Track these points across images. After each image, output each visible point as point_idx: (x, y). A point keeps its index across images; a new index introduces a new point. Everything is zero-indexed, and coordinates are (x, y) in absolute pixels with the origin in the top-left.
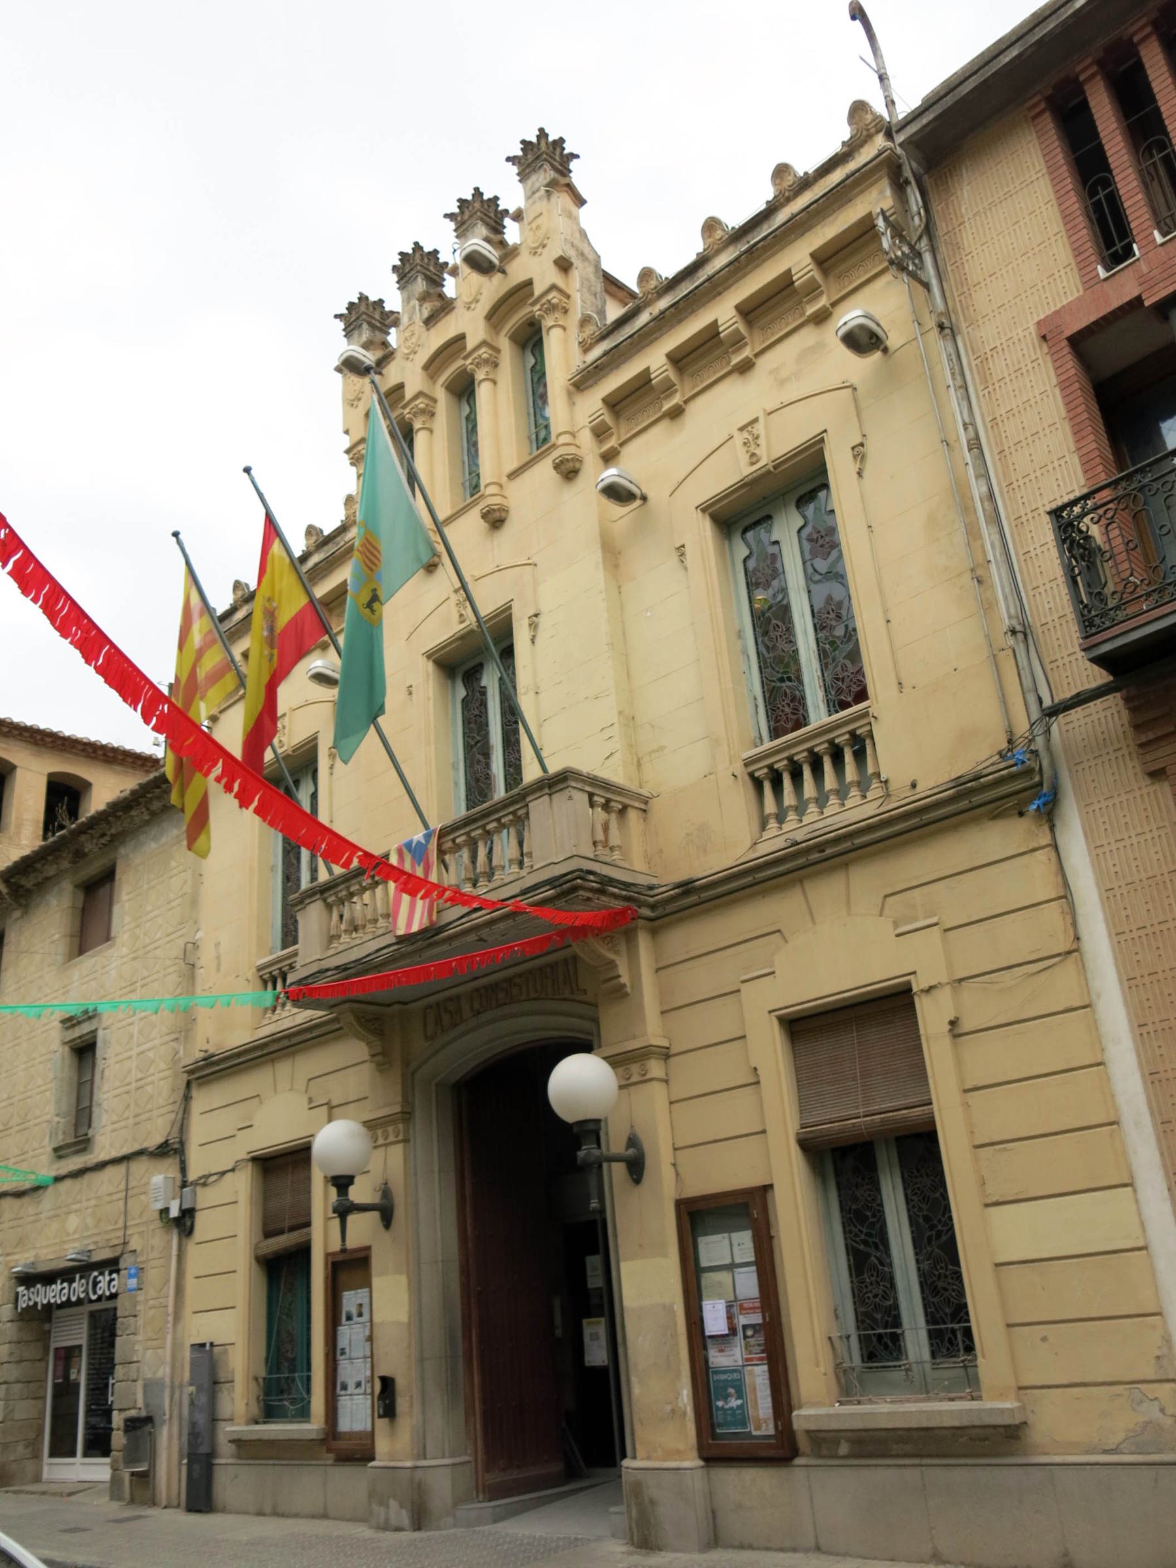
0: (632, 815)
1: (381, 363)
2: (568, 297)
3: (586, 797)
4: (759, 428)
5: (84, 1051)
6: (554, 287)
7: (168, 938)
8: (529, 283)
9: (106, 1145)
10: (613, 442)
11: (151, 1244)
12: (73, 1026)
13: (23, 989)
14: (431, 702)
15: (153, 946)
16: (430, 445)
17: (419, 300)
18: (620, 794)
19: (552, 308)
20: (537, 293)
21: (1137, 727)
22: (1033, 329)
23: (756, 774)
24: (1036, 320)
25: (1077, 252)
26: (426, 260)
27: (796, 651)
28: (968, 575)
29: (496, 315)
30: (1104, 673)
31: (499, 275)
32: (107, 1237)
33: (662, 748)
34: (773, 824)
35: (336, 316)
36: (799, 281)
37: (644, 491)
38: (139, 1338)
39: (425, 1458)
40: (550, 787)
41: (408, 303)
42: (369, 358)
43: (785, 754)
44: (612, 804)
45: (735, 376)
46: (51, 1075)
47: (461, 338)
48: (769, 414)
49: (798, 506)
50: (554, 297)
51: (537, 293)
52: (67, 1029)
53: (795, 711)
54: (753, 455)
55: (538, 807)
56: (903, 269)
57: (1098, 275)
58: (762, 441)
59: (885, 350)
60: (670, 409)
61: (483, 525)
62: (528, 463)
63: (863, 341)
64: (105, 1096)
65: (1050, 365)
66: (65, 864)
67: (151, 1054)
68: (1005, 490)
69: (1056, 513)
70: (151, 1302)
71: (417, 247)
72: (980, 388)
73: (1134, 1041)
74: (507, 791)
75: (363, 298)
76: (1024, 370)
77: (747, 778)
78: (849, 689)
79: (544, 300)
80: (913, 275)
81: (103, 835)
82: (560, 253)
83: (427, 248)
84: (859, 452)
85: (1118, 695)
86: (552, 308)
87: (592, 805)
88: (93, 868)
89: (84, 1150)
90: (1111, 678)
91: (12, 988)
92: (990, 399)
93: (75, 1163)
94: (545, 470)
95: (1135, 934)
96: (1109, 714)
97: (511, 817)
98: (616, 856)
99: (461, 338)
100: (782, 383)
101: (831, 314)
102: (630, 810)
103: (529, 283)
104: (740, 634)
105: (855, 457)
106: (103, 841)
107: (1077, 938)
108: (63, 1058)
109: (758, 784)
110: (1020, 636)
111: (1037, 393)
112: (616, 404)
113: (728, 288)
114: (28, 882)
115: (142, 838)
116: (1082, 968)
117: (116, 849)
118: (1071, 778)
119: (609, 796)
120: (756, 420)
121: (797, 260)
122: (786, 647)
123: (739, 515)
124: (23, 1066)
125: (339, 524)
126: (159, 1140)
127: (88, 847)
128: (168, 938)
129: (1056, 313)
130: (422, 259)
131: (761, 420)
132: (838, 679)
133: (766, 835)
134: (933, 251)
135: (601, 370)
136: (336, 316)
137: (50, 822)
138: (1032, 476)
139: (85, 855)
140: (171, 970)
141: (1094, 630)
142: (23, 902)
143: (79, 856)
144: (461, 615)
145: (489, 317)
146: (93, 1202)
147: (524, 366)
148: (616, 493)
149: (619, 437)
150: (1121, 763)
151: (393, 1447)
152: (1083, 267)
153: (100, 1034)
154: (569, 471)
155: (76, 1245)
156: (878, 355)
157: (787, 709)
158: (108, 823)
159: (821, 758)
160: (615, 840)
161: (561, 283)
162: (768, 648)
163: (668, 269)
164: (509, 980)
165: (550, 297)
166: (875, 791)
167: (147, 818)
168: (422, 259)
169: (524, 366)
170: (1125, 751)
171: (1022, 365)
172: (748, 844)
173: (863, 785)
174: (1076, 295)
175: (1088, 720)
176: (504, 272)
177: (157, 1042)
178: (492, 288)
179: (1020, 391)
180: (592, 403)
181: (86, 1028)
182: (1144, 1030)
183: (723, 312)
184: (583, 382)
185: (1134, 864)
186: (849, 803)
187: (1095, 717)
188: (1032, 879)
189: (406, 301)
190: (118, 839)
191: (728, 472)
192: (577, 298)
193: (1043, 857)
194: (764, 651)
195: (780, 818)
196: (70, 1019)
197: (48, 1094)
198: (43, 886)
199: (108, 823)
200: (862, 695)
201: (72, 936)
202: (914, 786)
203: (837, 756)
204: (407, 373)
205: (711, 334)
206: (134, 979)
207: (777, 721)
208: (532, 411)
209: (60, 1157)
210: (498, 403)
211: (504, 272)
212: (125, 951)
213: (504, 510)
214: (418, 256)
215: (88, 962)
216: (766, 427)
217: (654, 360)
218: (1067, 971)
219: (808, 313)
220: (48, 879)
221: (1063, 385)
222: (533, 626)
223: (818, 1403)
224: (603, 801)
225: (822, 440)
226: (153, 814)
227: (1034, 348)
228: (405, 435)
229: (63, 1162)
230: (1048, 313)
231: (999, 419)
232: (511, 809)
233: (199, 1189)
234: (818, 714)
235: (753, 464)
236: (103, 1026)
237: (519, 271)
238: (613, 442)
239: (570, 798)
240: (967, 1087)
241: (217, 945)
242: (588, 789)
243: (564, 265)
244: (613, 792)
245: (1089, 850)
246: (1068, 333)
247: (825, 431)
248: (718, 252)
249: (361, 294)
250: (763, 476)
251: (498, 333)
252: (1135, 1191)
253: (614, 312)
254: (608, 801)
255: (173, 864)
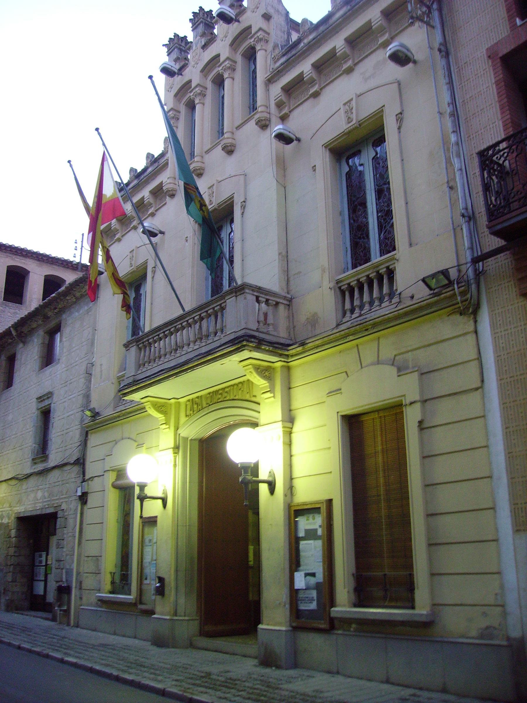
0: (281, 308)
1: (182, 69)
2: (269, 34)
3: (255, 298)
4: (354, 103)
5: (46, 414)
6: (260, 29)
7: (81, 361)
8: (250, 27)
9: (54, 459)
10: (286, 111)
11: (70, 506)
12: (42, 401)
13: (22, 382)
14: (196, 245)
15: (74, 364)
16: (203, 111)
17: (200, 36)
18: (274, 296)
19: (260, 40)
20: (253, 32)
21: (518, 270)
22: (485, 52)
23: (342, 288)
24: (487, 47)
25: (508, 10)
26: (206, 15)
27: (368, 223)
28: (446, 185)
29: (235, 43)
30: (503, 241)
31: (237, 23)
32: (53, 502)
33: (300, 272)
34: (348, 314)
35: (163, 45)
36: (375, 25)
37: (298, 136)
38: (65, 550)
39: (176, 616)
40: (236, 293)
41: (196, 38)
42: (176, 67)
43: (356, 278)
44: (270, 301)
45: (345, 75)
46: (33, 425)
47: (218, 56)
48: (359, 96)
49: (373, 146)
50: (260, 34)
51: (253, 32)
52: (40, 402)
53: (365, 255)
54: (349, 118)
55: (230, 302)
56: (422, 21)
57: (516, 23)
58: (354, 111)
59: (415, 62)
60: (382, 42)
61: (223, 153)
62: (242, 124)
63: (401, 58)
64: (54, 436)
65: (492, 70)
66: (40, 322)
67: (72, 417)
68: (467, 139)
69: (482, 154)
70: (70, 534)
71: (201, 8)
72: (458, 84)
73: (503, 435)
74: (212, 297)
75: (176, 35)
76: (479, 75)
77: (338, 290)
78: (388, 245)
79: (256, 36)
80: (428, 24)
81: (55, 308)
82: (265, 11)
83: (207, 9)
84: (400, 117)
85: (508, 252)
86: (260, 40)
87: (258, 301)
88: (52, 324)
89: (44, 461)
90: (506, 243)
91: (18, 381)
92: (463, 90)
93: (40, 467)
94: (252, 125)
95: (509, 380)
96: (503, 261)
97: (218, 307)
98: (271, 328)
99: (218, 56)
100: (366, 80)
101: (155, 214)
102: (280, 304)
103: (250, 27)
104: (341, 213)
105: (397, 120)
106: (56, 311)
107: (483, 381)
108: (37, 416)
109: (343, 293)
110: (467, 219)
111: (485, 87)
112: (288, 90)
113: (341, 29)
114: (25, 329)
115: (72, 310)
116: (483, 397)
117: (61, 315)
118: (486, 295)
119: (267, 297)
120: (352, 99)
121: (338, 42)
122: (364, 220)
123: (343, 151)
124: (22, 419)
125: (161, 152)
126: (75, 458)
127: (50, 314)
128: (81, 361)
129: (497, 44)
130: (204, 15)
131: (354, 99)
132: (386, 239)
133: (345, 320)
134: (440, 10)
135: (281, 72)
136: (163, 45)
137: (46, 292)
138: (480, 132)
139: (49, 318)
140: (81, 376)
141: (494, 218)
142: (23, 340)
143: (46, 318)
144: (211, 201)
145: (232, 45)
146: (47, 486)
147: (249, 70)
148: (283, 138)
149: (320, 85)
150: (510, 288)
151: (163, 610)
152: (511, 19)
153: (52, 405)
154: (264, 125)
155: (41, 505)
156: (411, 65)
157: (361, 254)
158: (57, 302)
159: (373, 280)
160: (270, 320)
161: (265, 27)
162: (354, 220)
163: (315, 20)
164: (223, 389)
165: (258, 34)
166: (395, 300)
167: (75, 300)
168: (204, 15)
169: (249, 70)
170: (512, 283)
171: (479, 72)
172: (334, 325)
173: (391, 295)
174: (506, 34)
175: (497, 265)
176: (239, 21)
177: (75, 411)
178: (235, 29)
179: (477, 87)
180: (276, 89)
181: (47, 402)
182: (508, 430)
183: (338, 42)
184: (270, 81)
185: (511, 343)
186: (383, 305)
187: (500, 264)
188: (465, 349)
189: (195, 37)
190: (62, 311)
191: (338, 127)
192: (272, 33)
193: (471, 338)
194: (352, 221)
195: (352, 311)
196: (40, 397)
197: (31, 433)
198: (32, 331)
199: (57, 302)
200: (394, 249)
201: (42, 357)
202: (412, 297)
203: (380, 278)
204: (193, 74)
205: (332, 53)
206: (66, 380)
207: (356, 260)
208: (252, 93)
209: (35, 463)
210: (234, 90)
211: (239, 21)
212: (63, 366)
213: (233, 146)
214: (201, 13)
215: (49, 370)
216: (357, 103)
217: (305, 67)
218: (475, 398)
219: (310, 93)
220: (33, 329)
221: (497, 83)
222: (243, 207)
223: (344, 605)
224: (265, 300)
225: (382, 111)
226: (78, 299)
227: (485, 63)
228: (191, 106)
229: (35, 466)
230: (492, 43)
231: (466, 101)
232: (219, 303)
233: (90, 482)
234: (376, 258)
235: (349, 123)
236: (54, 402)
237: (247, 19)
238: (286, 111)
239: (245, 298)
240: (424, 455)
241: (101, 365)
242: (256, 294)
243: (267, 17)
244: (271, 296)
245: (492, 335)
246: (500, 55)
247: (384, 106)
248: (339, 10)
249: (175, 34)
250: (354, 129)
251: (236, 53)
252: (495, 512)
253: (295, 37)
254: (267, 300)
255: (85, 324)
